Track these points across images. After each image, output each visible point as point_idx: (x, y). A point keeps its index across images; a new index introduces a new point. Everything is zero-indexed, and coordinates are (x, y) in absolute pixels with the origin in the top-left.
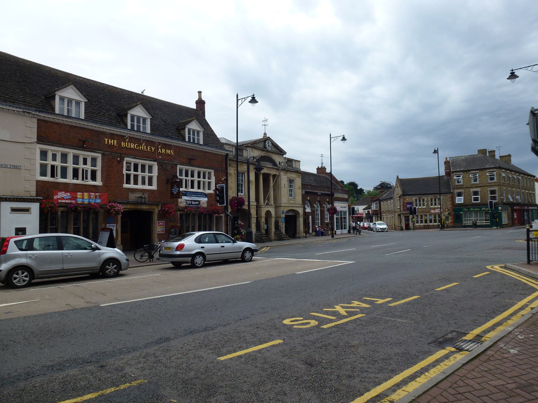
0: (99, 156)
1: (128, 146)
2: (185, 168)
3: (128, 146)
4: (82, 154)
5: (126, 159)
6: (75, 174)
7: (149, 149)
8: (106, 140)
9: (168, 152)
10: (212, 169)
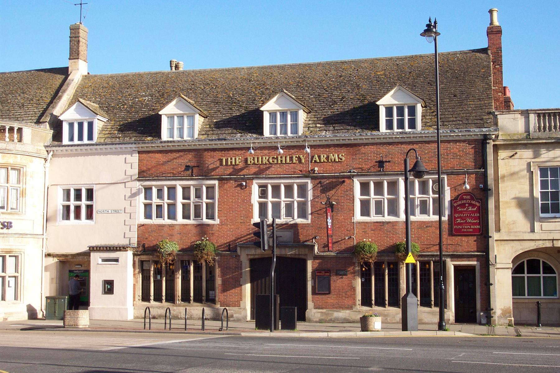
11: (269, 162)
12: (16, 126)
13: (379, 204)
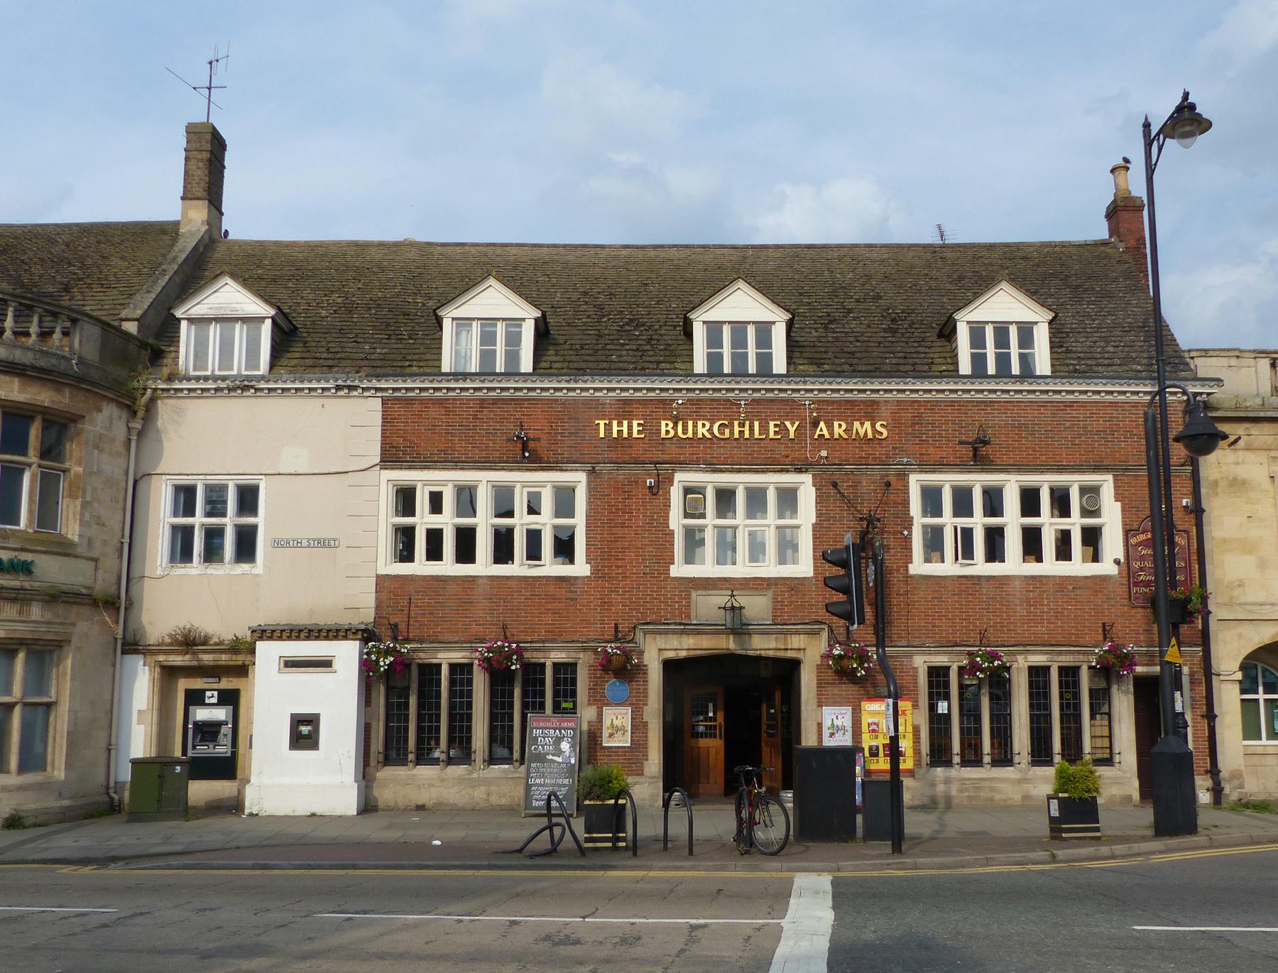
0: (578, 479)
1: (685, 431)
2: (947, 481)
3: (685, 431)
4: (521, 480)
5: (682, 478)
6: (503, 550)
7: (772, 429)
8: (602, 423)
9: (864, 428)
10: (1097, 469)
11: (712, 434)
12: (448, 566)
13: (435, 537)
